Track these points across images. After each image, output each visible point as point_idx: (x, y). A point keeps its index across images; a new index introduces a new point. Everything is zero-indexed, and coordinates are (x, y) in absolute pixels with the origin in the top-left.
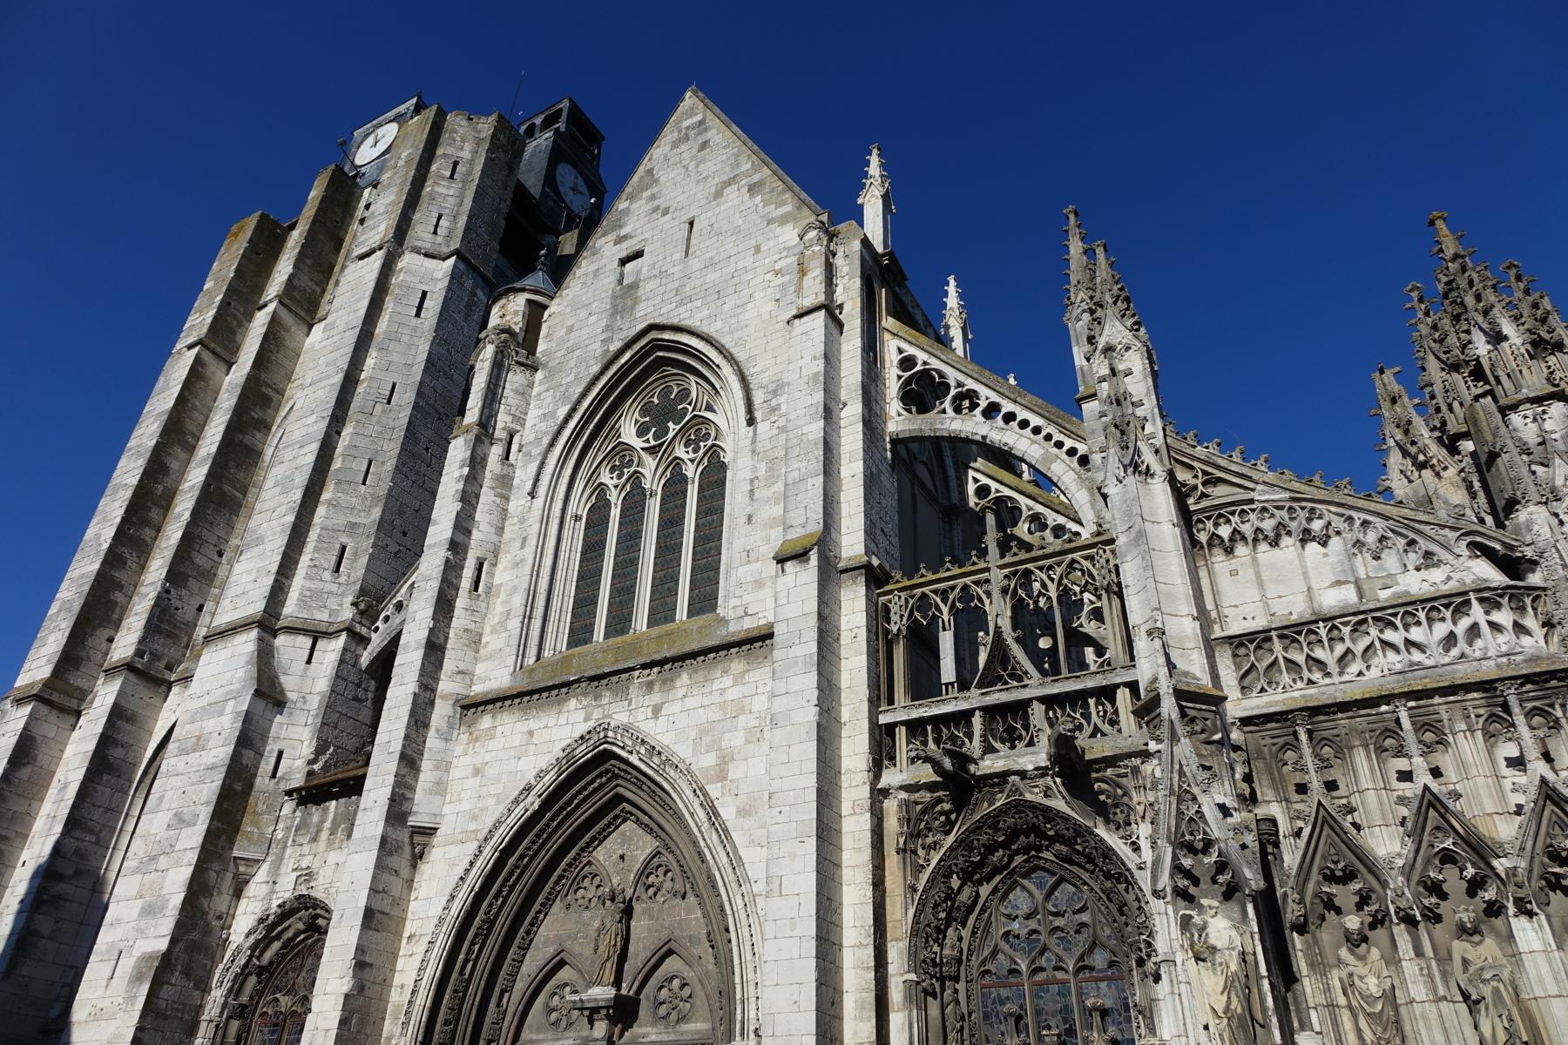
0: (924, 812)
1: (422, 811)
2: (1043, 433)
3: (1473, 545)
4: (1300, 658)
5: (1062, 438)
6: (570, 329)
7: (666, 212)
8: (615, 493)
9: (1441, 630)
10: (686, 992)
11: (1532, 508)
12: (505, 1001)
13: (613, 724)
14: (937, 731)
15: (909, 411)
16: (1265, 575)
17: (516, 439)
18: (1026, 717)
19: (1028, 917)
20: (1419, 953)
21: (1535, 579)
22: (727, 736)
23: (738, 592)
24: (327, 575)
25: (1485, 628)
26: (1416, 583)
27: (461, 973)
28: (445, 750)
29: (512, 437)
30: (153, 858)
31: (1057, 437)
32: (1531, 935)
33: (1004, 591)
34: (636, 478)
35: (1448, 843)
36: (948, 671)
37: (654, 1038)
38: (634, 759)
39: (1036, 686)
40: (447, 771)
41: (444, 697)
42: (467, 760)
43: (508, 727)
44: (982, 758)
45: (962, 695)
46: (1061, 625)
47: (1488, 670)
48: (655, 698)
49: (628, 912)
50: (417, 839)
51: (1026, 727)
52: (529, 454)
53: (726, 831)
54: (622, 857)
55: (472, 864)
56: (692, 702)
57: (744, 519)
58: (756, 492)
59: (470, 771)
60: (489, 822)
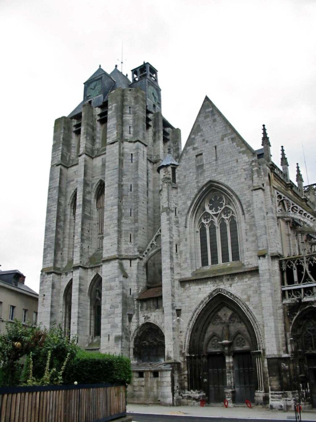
6: (185, 177)
7: (207, 142)
8: (207, 226)
10: (243, 341)
14: (294, 291)
24: (129, 243)
29: (176, 209)
33: (307, 262)
34: (212, 222)
41: (176, 280)
43: (194, 288)
44: (303, 298)
48: (230, 282)
52: (181, 214)
55: (192, 317)
56: (239, 284)
57: (245, 240)
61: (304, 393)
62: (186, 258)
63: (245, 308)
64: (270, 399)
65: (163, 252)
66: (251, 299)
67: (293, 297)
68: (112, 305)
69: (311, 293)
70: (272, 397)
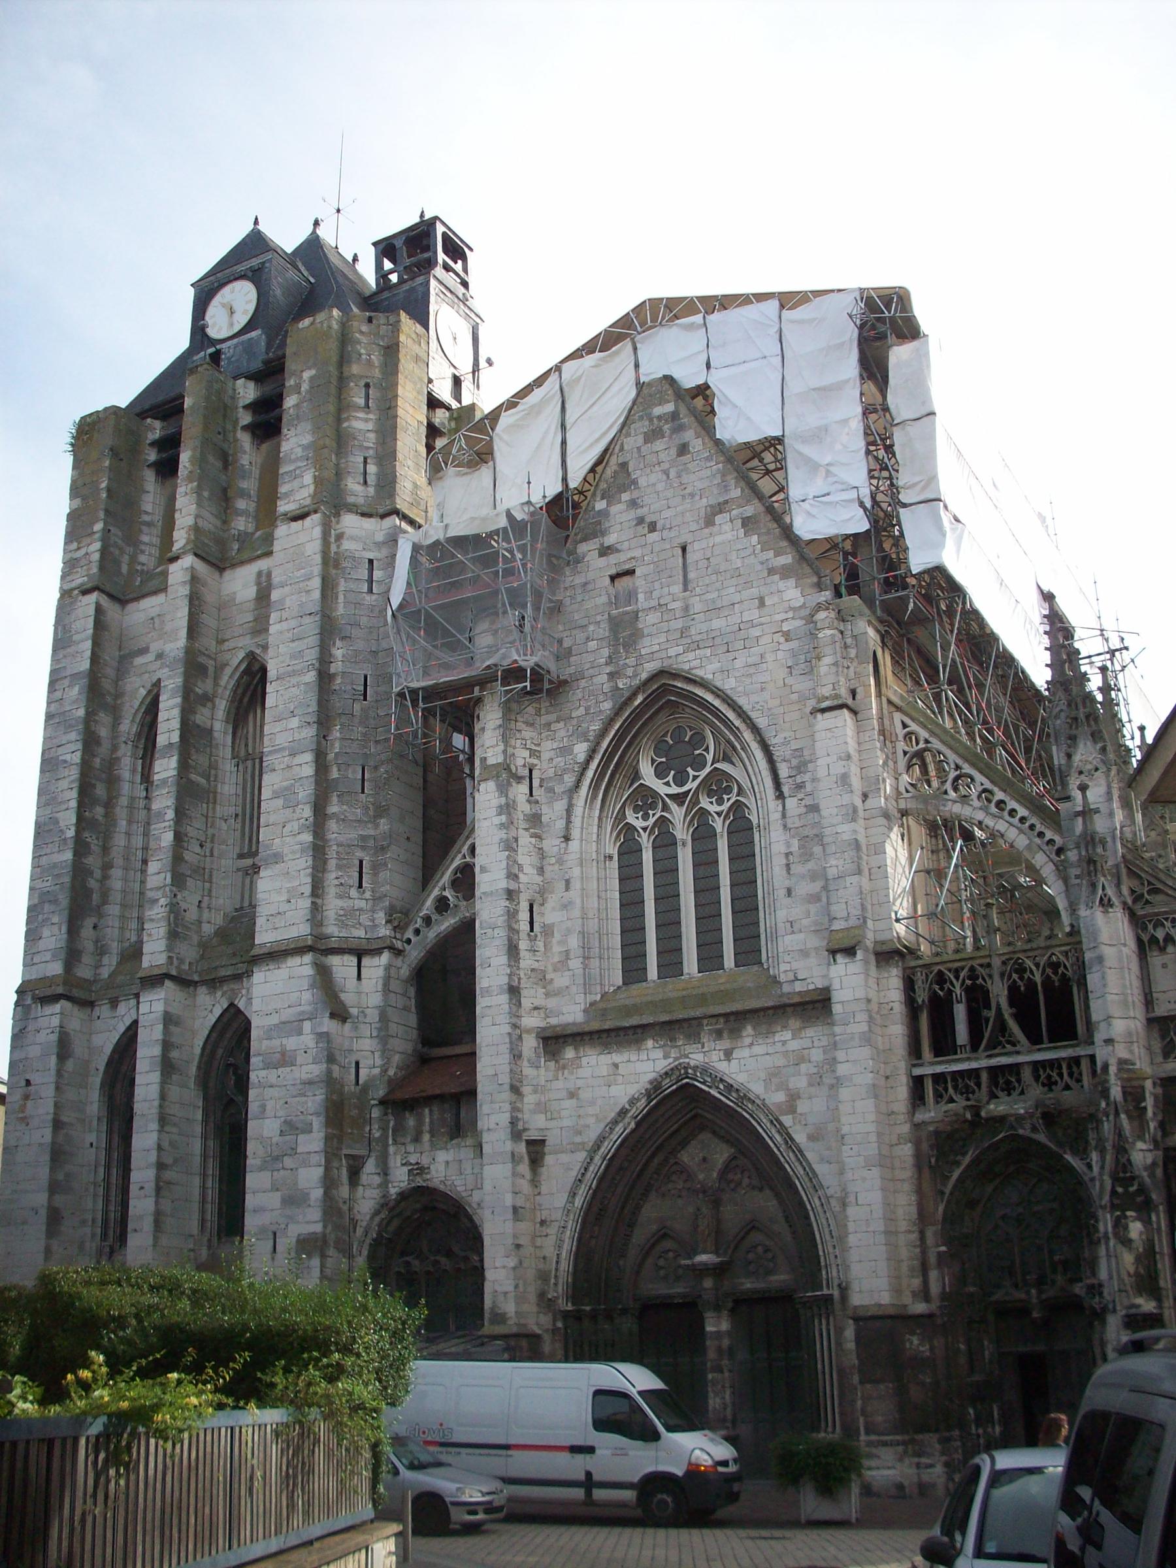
7: (652, 527)
8: (645, 836)
10: (770, 1255)
17: (535, 774)
18: (1018, 1074)
22: (792, 1079)
23: (787, 958)
24: (354, 893)
29: (531, 771)
30: (277, 1158)
31: (1039, 827)
33: (1002, 975)
34: (663, 822)
37: (749, 1286)
39: (1028, 1056)
43: (594, 1063)
48: (725, 1044)
51: (1019, 1081)
53: (800, 1151)
54: (704, 1159)
56: (757, 1050)
58: (792, 867)
59: (564, 1094)
66: (802, 1106)
67: (951, 1100)
68: (285, 1122)
69: (1014, 1088)
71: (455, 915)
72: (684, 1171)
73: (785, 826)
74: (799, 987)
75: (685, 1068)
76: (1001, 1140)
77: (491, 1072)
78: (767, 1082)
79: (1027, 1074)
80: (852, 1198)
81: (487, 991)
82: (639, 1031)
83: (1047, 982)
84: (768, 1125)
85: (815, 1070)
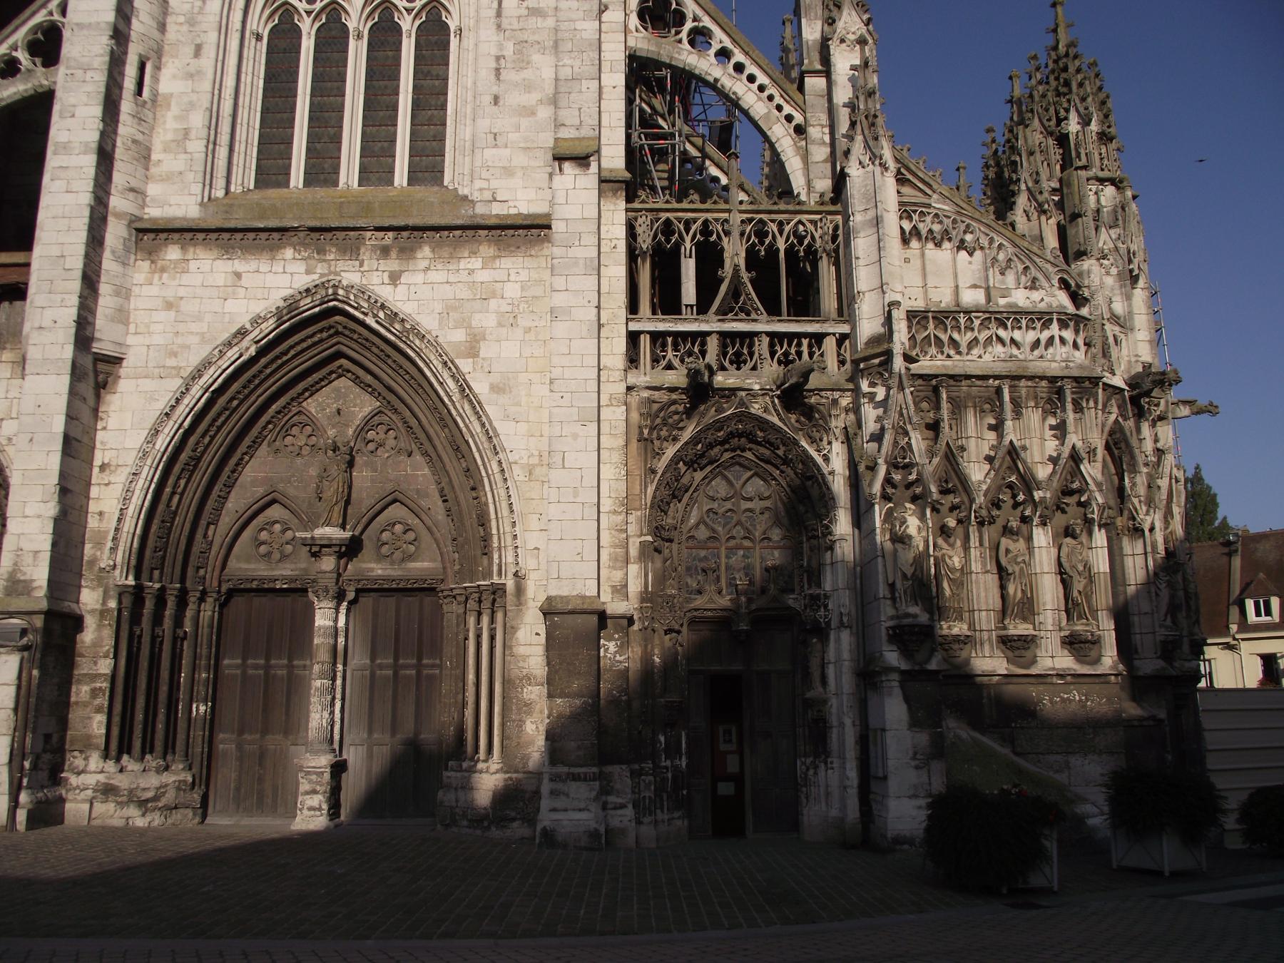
0: (661, 410)
1: (106, 337)
2: (766, 93)
3: (1062, 281)
4: (944, 338)
5: (782, 102)
9: (1031, 336)
10: (411, 536)
11: (1093, 261)
12: (210, 533)
13: (345, 283)
15: (646, 29)
16: (928, 268)
19: (726, 500)
20: (981, 544)
21: (1084, 311)
22: (477, 316)
25: (1057, 340)
26: (1021, 298)
27: (168, 506)
28: (124, 275)
32: (1042, 538)
35: (1013, 479)
36: (689, 292)
37: (380, 572)
38: (370, 321)
40: (128, 298)
41: (119, 216)
42: (154, 290)
43: (206, 269)
45: (701, 317)
46: (793, 277)
47: (1054, 369)
48: (393, 264)
49: (351, 464)
50: (101, 366)
51: (751, 354)
54: (339, 412)
55: (178, 401)
56: (434, 276)
58: (503, 72)
60: (194, 360)
61: (670, 775)
62: (186, 133)
63: (451, 384)
64: (545, 803)
65: (61, 117)
66: (486, 350)
67: (669, 367)
69: (745, 362)
70: (554, 793)
71: (26, 80)
72: (309, 422)
73: (499, 26)
74: (497, 209)
75: (334, 286)
76: (728, 418)
77: (55, 251)
78: (444, 315)
79: (763, 346)
80: (557, 459)
81: (65, 148)
82: (276, 235)
83: (790, 251)
84: (440, 367)
85: (509, 308)
